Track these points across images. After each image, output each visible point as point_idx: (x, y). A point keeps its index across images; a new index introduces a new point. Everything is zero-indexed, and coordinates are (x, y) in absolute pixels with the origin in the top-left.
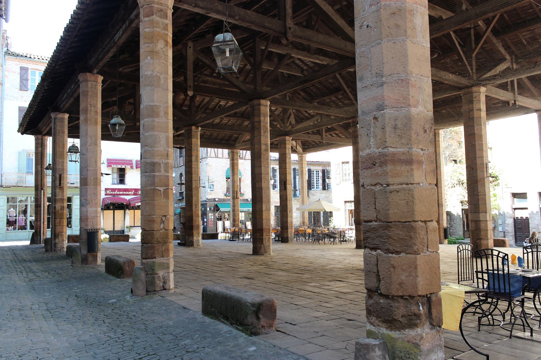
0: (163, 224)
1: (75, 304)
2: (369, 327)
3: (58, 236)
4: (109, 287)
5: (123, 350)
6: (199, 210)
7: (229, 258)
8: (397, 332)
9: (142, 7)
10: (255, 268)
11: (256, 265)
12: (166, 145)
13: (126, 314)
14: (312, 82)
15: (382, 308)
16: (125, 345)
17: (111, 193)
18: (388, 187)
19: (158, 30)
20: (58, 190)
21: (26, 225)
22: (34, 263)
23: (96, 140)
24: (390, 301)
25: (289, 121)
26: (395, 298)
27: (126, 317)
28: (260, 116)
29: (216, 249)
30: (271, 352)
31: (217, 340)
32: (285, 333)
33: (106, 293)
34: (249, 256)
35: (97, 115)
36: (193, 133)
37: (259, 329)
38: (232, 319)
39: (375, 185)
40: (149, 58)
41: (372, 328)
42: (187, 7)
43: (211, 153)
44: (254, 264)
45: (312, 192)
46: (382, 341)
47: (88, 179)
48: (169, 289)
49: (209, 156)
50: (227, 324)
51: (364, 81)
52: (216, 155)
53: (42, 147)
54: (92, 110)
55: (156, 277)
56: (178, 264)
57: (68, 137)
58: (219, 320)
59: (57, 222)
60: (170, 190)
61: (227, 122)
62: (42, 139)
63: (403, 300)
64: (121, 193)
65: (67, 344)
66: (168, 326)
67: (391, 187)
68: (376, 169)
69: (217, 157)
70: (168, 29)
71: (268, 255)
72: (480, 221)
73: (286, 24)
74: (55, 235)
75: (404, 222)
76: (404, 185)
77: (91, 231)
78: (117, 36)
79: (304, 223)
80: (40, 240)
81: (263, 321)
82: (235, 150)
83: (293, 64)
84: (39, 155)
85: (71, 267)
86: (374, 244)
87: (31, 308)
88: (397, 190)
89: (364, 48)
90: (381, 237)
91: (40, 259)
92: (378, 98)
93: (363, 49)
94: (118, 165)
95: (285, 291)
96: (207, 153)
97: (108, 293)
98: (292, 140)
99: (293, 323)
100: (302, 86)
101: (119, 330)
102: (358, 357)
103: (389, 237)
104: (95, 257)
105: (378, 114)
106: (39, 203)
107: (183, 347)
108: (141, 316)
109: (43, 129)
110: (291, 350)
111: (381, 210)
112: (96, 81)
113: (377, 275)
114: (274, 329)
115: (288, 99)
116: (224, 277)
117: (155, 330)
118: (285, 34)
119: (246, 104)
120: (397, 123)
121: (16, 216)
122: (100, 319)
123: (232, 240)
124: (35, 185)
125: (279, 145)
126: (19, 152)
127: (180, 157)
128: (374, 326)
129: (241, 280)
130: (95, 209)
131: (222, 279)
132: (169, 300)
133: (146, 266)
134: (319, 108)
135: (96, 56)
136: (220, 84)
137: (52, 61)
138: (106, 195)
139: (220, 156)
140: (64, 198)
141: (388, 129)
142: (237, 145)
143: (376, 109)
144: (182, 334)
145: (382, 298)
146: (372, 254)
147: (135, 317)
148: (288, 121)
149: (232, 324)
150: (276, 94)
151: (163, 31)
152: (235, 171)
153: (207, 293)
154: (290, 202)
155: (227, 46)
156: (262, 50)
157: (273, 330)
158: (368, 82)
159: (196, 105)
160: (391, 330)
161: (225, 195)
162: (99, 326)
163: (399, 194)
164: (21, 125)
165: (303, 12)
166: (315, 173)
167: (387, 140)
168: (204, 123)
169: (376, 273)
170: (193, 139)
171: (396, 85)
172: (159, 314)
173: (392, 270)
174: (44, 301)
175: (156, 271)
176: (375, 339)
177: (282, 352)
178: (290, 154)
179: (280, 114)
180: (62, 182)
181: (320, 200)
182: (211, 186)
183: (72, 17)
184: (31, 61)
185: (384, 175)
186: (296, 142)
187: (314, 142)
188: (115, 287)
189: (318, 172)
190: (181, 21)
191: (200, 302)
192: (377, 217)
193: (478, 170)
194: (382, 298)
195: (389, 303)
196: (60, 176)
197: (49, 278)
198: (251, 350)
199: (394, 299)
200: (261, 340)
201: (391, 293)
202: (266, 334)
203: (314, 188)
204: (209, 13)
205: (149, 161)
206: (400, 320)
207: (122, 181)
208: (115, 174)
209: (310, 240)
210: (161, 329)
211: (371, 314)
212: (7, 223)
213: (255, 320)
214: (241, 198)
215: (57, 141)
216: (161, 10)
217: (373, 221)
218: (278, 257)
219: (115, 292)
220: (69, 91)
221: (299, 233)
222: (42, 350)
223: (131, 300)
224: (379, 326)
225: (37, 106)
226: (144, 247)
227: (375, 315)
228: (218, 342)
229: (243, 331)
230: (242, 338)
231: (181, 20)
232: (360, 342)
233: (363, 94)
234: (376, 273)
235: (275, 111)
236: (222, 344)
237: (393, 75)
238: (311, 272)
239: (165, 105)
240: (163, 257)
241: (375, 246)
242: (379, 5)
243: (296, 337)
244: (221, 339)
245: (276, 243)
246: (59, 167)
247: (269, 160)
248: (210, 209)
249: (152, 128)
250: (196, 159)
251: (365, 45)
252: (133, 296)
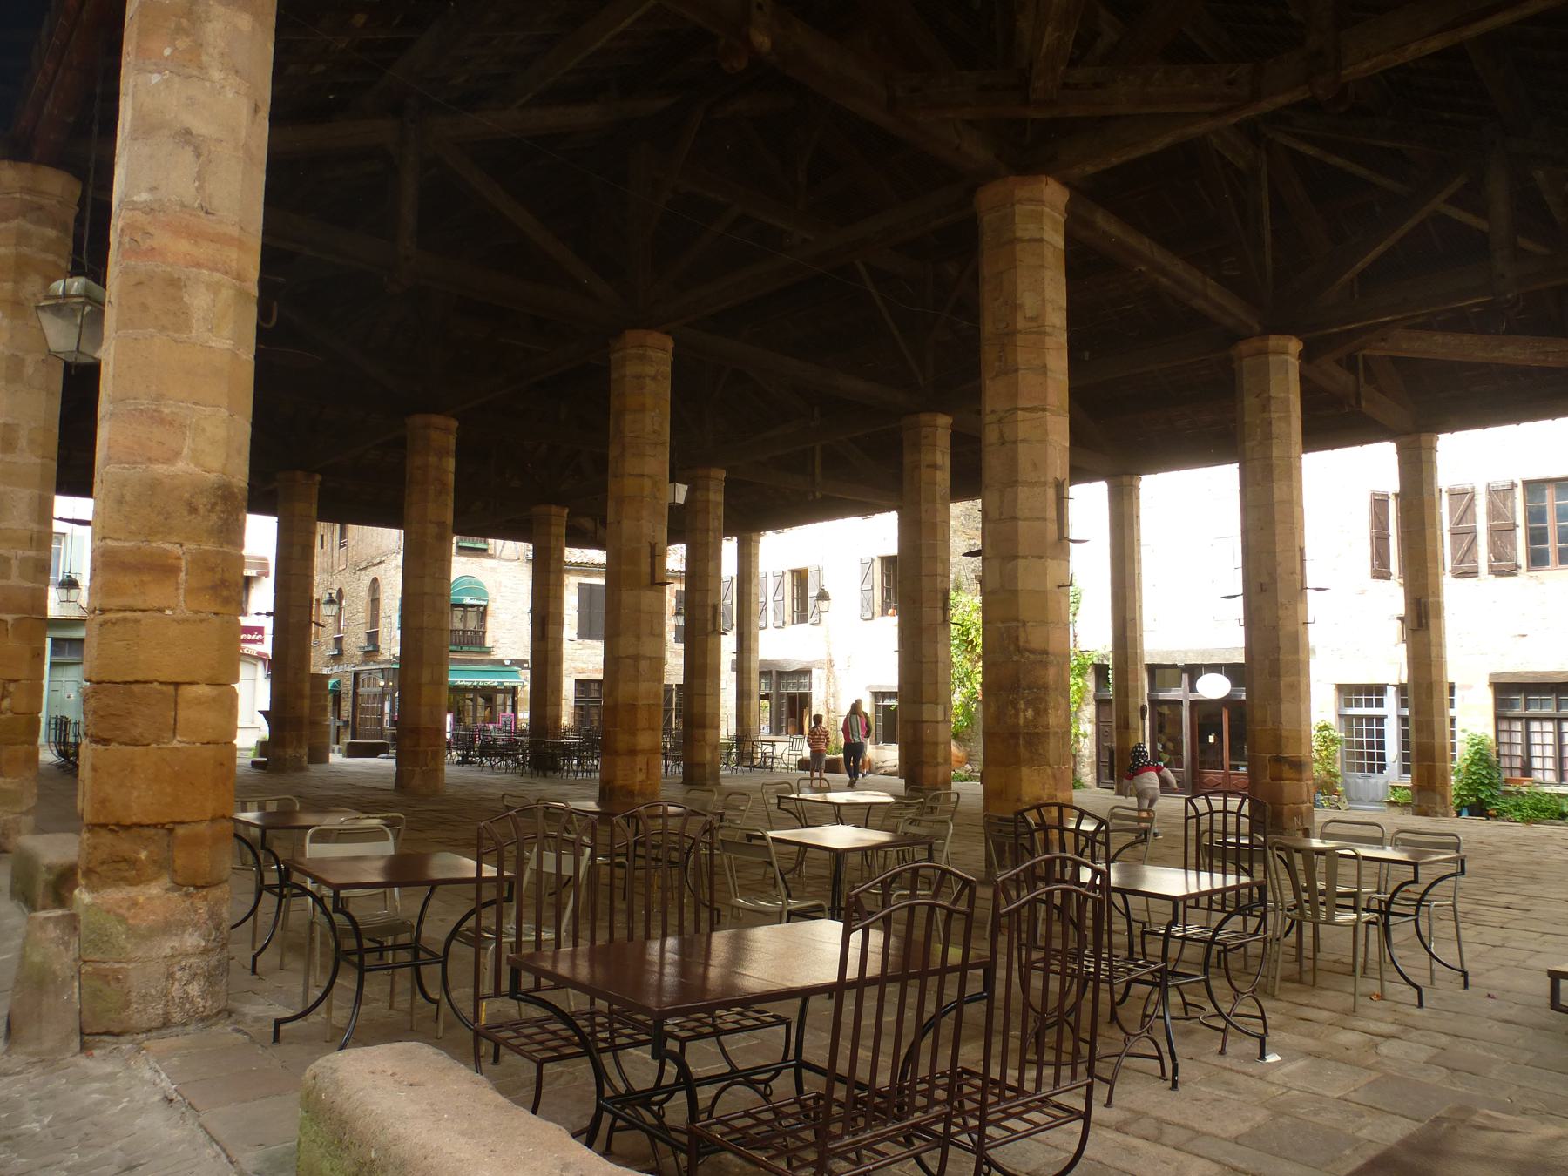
72: (923, 722)
120: (125, 492)
127: (341, 547)
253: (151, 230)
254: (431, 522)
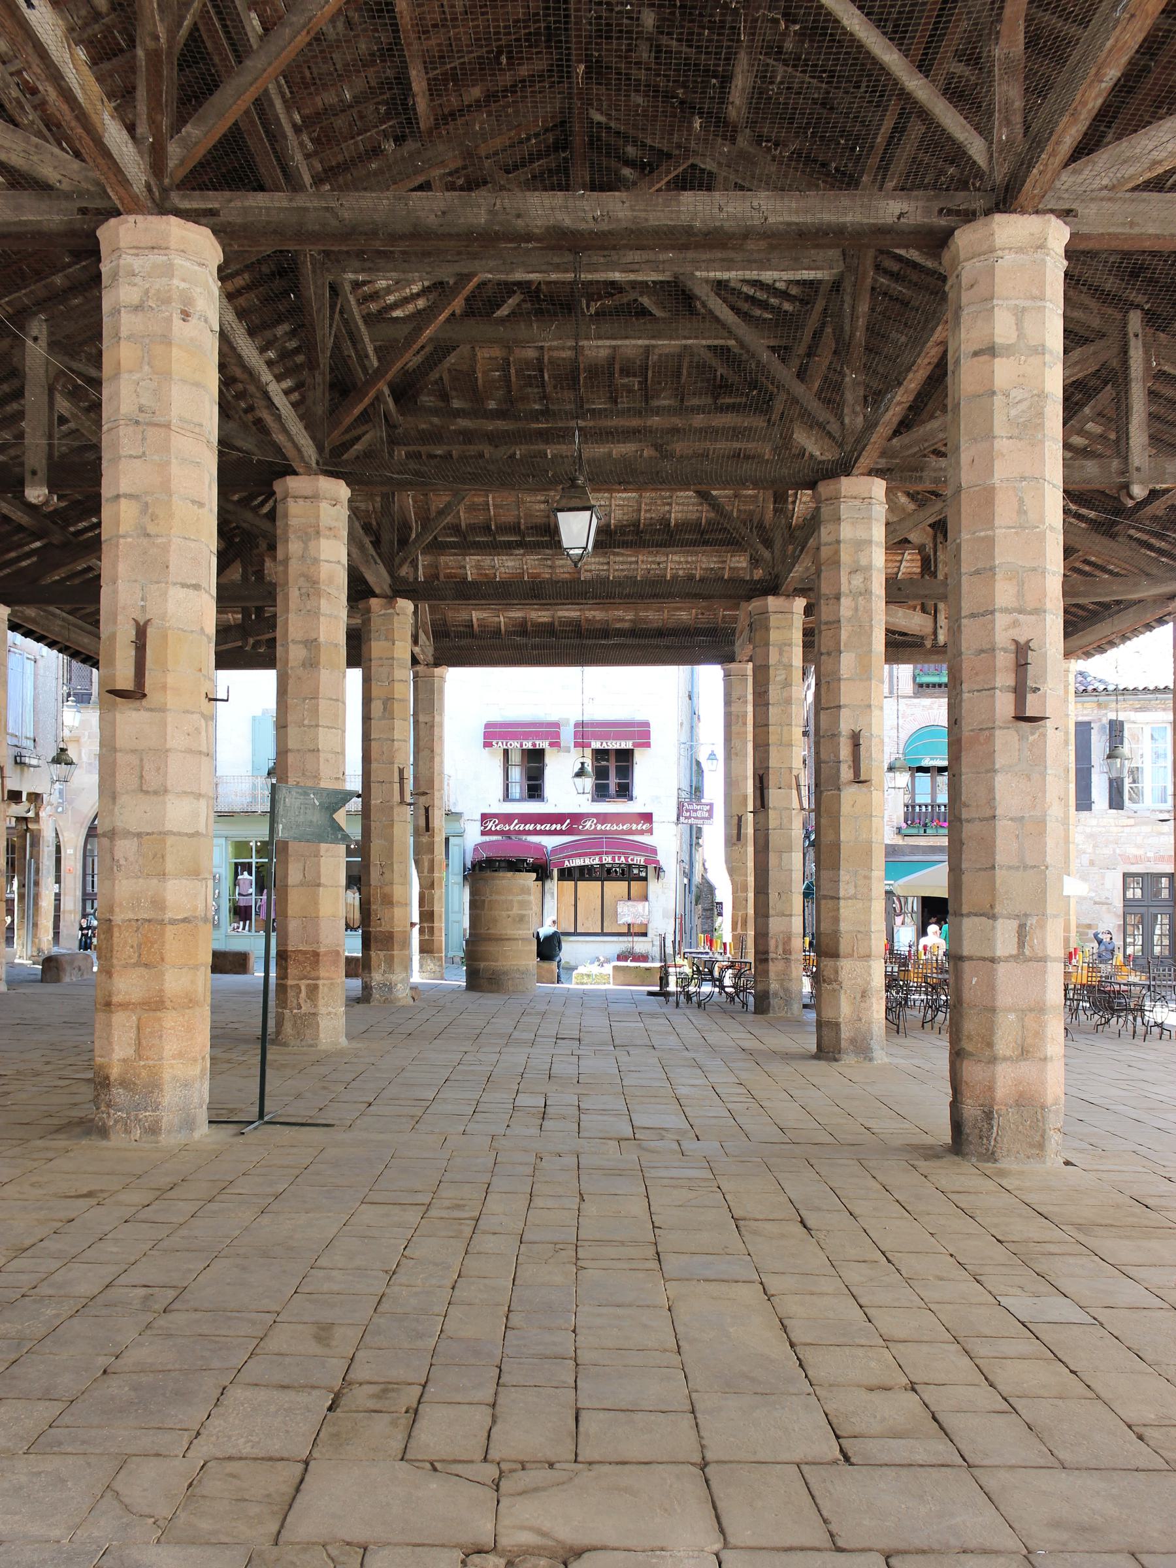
64: (530, 827)
126: (254, 718)
138: (483, 833)
170: (373, 643)
193: (965, 687)
207: (535, 791)
250: (385, 709)
254: (294, 642)
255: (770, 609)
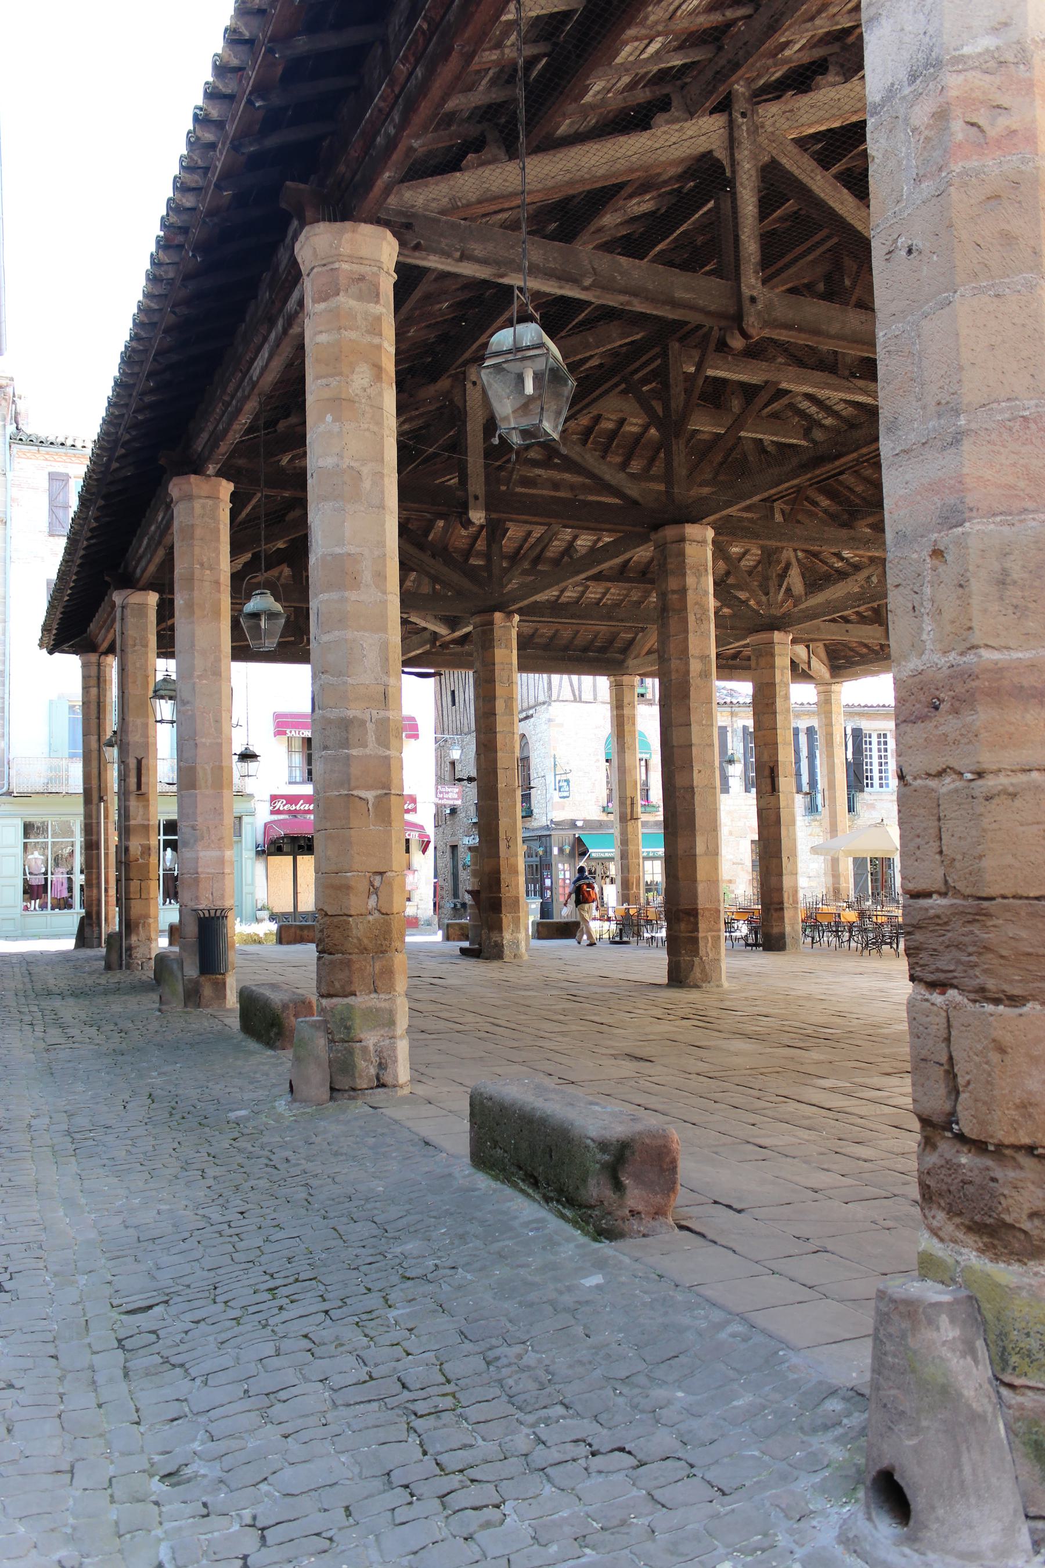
0: (374, 897)
1: (141, 1118)
2: (927, 1243)
3: (137, 926)
4: (240, 1073)
5: (232, 1260)
6: (516, 856)
7: (597, 996)
8: (1016, 1267)
9: (308, 275)
10: (664, 1027)
11: (671, 1017)
12: (382, 667)
13: (266, 1153)
14: (837, 463)
15: (964, 1182)
16: (241, 1245)
17: (286, 808)
18: (980, 782)
19: (353, 335)
20: (133, 803)
21: (71, 897)
22: (71, 1001)
23: (218, 660)
24: (990, 1163)
25: (785, 584)
26: (1007, 1152)
27: (267, 1161)
28: (684, 575)
29: (567, 968)
30: (646, 1296)
31: (496, 1247)
32: (703, 1236)
33: (228, 1090)
34: (658, 990)
35: (219, 592)
36: (498, 633)
37: (623, 1219)
38: (548, 1184)
39: (940, 774)
40: (329, 418)
41: (936, 1248)
42: (439, 262)
43: (560, 690)
44: (664, 1013)
45: (863, 798)
46: (963, 1293)
47: (199, 770)
48: (395, 1086)
49: (554, 697)
50: (534, 1200)
51: (900, 433)
52: (577, 693)
53: (99, 687)
54: (205, 578)
55: (357, 1051)
56: (447, 1010)
57: (158, 657)
58: (515, 1186)
59: (132, 889)
60: (393, 798)
61: (598, 596)
62: (99, 665)
63: (1036, 1160)
65: (93, 1235)
66: (370, 1196)
67: (991, 782)
68: (942, 720)
69: (577, 699)
70: (381, 331)
71: (715, 989)
73: (739, 287)
74: (129, 925)
75: (1037, 898)
76: (1035, 775)
77: (207, 915)
78: (259, 363)
79: (836, 892)
80: (100, 938)
81: (635, 1196)
82: (626, 679)
83: (790, 414)
84: (93, 707)
85: (158, 1013)
86: (938, 970)
87: (29, 1126)
88: (1011, 790)
89: (899, 322)
90: (959, 946)
91: (87, 989)
92: (944, 486)
93: (896, 328)
94: (302, 731)
95: (738, 1100)
96: (550, 688)
97: (232, 1090)
98: (794, 641)
99: (735, 1206)
100: (809, 476)
101: (236, 1202)
102: (881, 1341)
103: (985, 947)
104: (220, 988)
105: (944, 538)
106: (94, 838)
107: (398, 1261)
108: (303, 1161)
109: (100, 637)
110: (708, 1292)
111: (959, 857)
112: (215, 498)
113: (947, 1072)
114: (672, 1223)
115: (778, 517)
116: (565, 1052)
117: (331, 1206)
118: (737, 319)
119: (644, 539)
120: (1008, 565)
121: (46, 873)
122: (195, 1166)
123: (618, 941)
124: (85, 789)
125: (753, 658)
126: (51, 702)
128: (942, 1240)
129: (613, 1062)
130: (218, 853)
131: (559, 1058)
132: (390, 1118)
133: (328, 1019)
134: (868, 542)
135: (211, 428)
136: (572, 487)
137: (100, 448)
138: (272, 813)
139: (587, 695)
140: (151, 823)
141: (976, 586)
142: (631, 662)
143: (940, 521)
144: (400, 1224)
145: (965, 1150)
146: (933, 1004)
147: (286, 1165)
148: (780, 586)
149: (547, 1200)
150: (729, 504)
151: (368, 338)
152: (628, 738)
153: (482, 1103)
154: (788, 830)
155: (528, 363)
156: (688, 377)
157: (666, 1224)
158: (912, 437)
159: (505, 550)
160: (996, 1258)
161: (604, 811)
162: (188, 1184)
163: (1018, 803)
164: (46, 628)
165: (809, 251)
166: (874, 740)
167: (974, 624)
168: (526, 602)
169: (946, 1067)
171: (1005, 436)
172: (354, 1158)
173: (994, 1057)
174: (68, 1107)
175: (358, 1031)
176: (943, 1283)
177: (679, 1298)
178: (787, 686)
179: (755, 567)
180: (143, 779)
181: (885, 822)
182: (561, 784)
183: (138, 324)
184: (75, 456)
185: (966, 740)
186: (808, 647)
187: (866, 646)
188: (255, 1072)
189: (885, 736)
190: (440, 309)
191: (466, 1125)
192: (946, 882)
194: (965, 1150)
195: (988, 1169)
196: (139, 762)
197: (97, 1042)
198: (587, 1285)
199: (1004, 1155)
200: (624, 1254)
201: (992, 1137)
202: (644, 1236)
203: (872, 786)
204: (502, 276)
205: (333, 714)
206: (1022, 1226)
208: (297, 755)
209: (853, 944)
210: (347, 1205)
211: (931, 1198)
212: (25, 892)
213: (609, 1193)
214: (644, 818)
215: (130, 668)
216: (362, 278)
217: (935, 892)
218: (744, 995)
219: (251, 1087)
220: (153, 528)
221: (814, 923)
222: (24, 1246)
223: (287, 1114)
224: (955, 1242)
225: (76, 574)
226: (324, 964)
227: (943, 1204)
228: (499, 1253)
229: (577, 1222)
230: (572, 1245)
231: (438, 306)
232: (890, 1291)
233: (897, 477)
234: (946, 1067)
235: (740, 560)
236: (509, 1261)
237: (995, 406)
238: (834, 1044)
239: (376, 553)
240: (376, 991)
241: (942, 976)
242: (944, 174)
243: (734, 1251)
244: (506, 1246)
245: (748, 951)
246: (134, 738)
247: (714, 705)
248: (561, 850)
249: (340, 621)
251: (903, 312)
252: (294, 1100)
253: (1005, 100)
255: (775, 641)
